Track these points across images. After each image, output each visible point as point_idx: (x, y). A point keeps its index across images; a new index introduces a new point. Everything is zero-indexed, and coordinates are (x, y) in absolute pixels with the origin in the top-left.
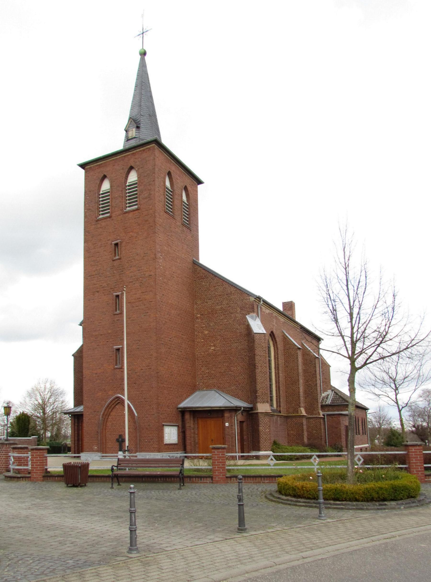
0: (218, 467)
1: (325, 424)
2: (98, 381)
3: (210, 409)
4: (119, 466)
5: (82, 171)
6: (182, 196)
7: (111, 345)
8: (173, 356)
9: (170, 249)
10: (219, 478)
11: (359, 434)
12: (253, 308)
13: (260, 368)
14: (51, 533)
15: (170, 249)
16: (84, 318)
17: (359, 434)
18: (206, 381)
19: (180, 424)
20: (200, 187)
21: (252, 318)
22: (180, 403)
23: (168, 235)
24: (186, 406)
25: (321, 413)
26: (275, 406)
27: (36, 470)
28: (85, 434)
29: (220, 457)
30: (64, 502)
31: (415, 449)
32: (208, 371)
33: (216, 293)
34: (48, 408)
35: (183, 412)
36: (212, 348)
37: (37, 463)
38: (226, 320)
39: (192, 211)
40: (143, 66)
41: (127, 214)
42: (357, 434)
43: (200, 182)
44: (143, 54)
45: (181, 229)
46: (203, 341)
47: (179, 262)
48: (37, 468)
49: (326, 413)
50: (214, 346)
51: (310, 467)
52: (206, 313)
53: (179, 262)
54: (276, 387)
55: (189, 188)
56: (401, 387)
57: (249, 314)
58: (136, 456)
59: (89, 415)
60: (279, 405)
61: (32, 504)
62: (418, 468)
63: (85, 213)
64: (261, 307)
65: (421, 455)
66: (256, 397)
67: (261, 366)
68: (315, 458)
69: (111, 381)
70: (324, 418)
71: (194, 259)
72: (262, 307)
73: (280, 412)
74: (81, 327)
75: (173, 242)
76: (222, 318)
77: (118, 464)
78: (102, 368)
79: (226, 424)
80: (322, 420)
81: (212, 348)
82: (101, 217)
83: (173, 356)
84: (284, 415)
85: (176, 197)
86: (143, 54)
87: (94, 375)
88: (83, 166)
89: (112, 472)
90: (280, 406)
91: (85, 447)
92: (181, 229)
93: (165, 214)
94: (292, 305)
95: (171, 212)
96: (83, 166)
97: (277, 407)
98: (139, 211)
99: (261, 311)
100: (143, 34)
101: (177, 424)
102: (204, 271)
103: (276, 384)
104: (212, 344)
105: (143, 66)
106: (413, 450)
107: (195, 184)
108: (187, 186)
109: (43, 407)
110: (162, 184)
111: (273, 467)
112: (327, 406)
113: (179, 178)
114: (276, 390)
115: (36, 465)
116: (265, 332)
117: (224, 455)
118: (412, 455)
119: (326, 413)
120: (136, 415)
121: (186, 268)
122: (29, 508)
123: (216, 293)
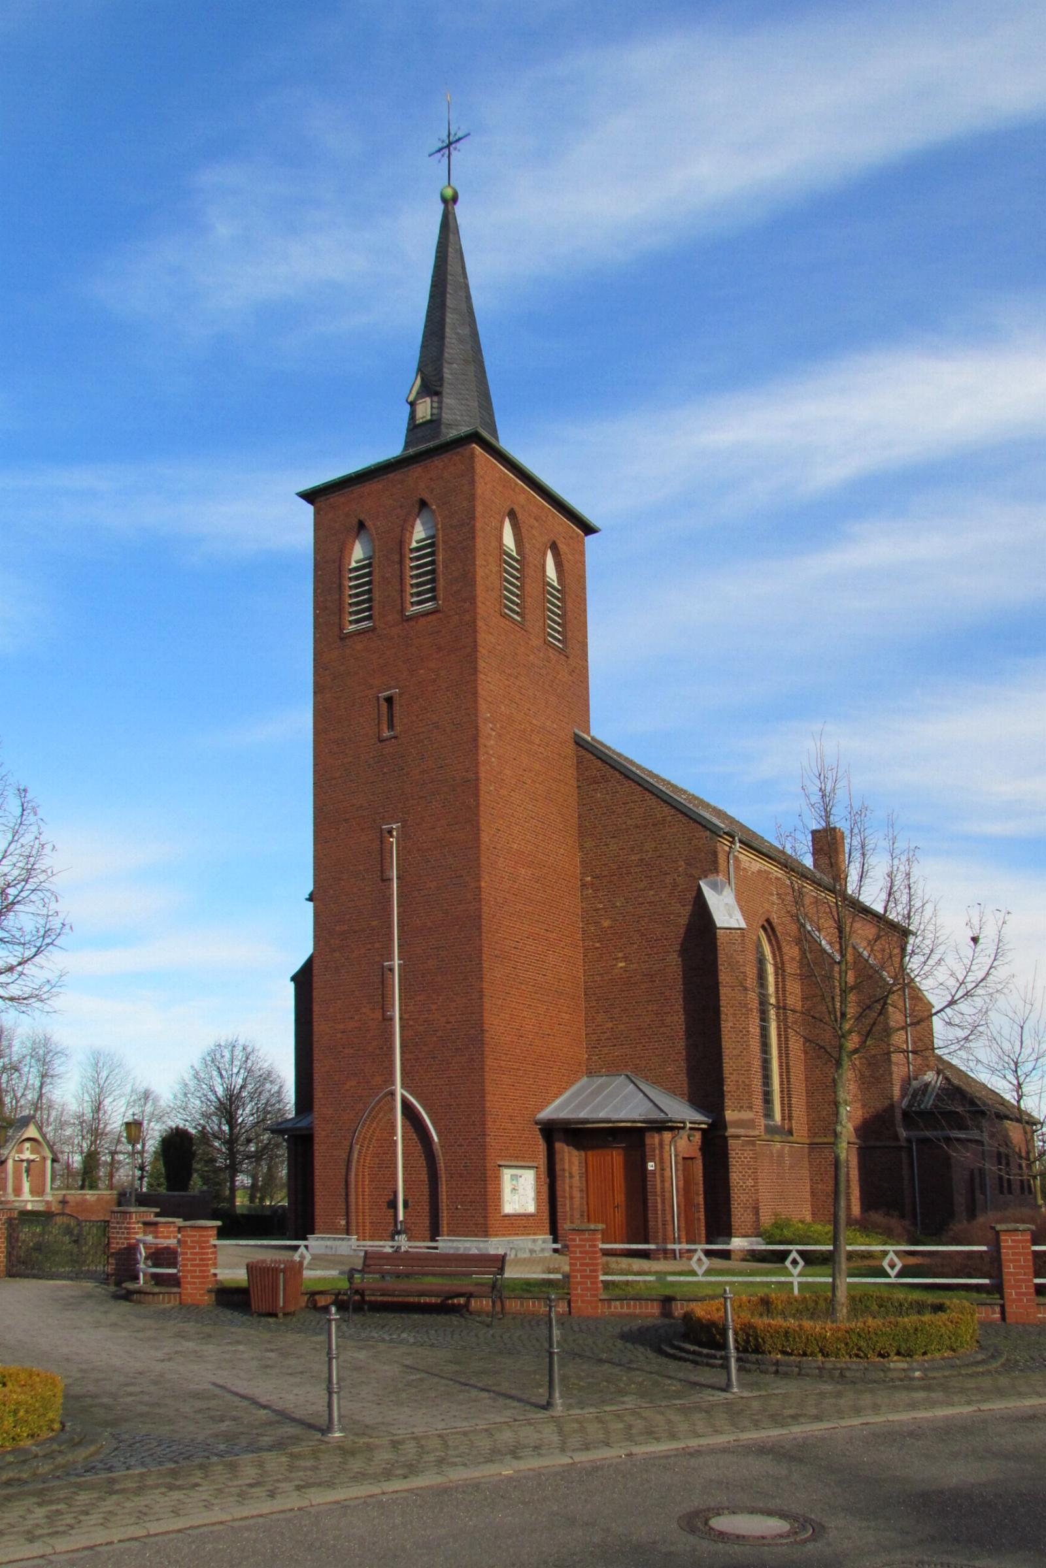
0: (582, 1277)
1: (911, 1165)
2: (346, 1051)
3: (629, 1125)
4: (367, 1269)
5: (310, 509)
6: (544, 571)
7: (377, 959)
8: (523, 987)
9: (513, 711)
10: (583, 1301)
11: (1010, 1192)
12: (715, 862)
13: (731, 1018)
14: (198, 1404)
15: (513, 711)
16: (315, 887)
17: (1010, 1192)
18: (605, 1050)
19: (542, 1160)
20: (590, 540)
21: (714, 887)
22: (542, 1109)
23: (510, 675)
24: (554, 1116)
25: (903, 1133)
26: (778, 1116)
27: (193, 1277)
28: (318, 1186)
29: (586, 1252)
30: (241, 1348)
31: (1013, 1241)
32: (610, 1025)
33: (629, 822)
34: (240, 1112)
35: (553, 1132)
36: (621, 965)
37: (1016, 1247)
38: (652, 893)
39: (570, 605)
40: (448, 227)
41: (412, 623)
42: (1002, 1192)
43: (588, 529)
44: (449, 202)
45: (541, 655)
46: (598, 945)
47: (537, 741)
48: (195, 1271)
49: (915, 1134)
50: (625, 959)
51: (783, 1279)
52: (606, 873)
53: (537, 741)
54: (781, 1066)
55: (563, 547)
56: (1028, 1080)
57: (706, 877)
58: (436, 1248)
59: (327, 1136)
60: (788, 1115)
61: (176, 1352)
62: (1020, 1287)
63: (316, 617)
64: (736, 859)
65: (1027, 1254)
66: (721, 1095)
67: (734, 1015)
68: (700, 1259)
69: (378, 1052)
70: (910, 1149)
71: (577, 731)
72: (741, 856)
73: (790, 1132)
74: (311, 904)
75: (523, 691)
76: (641, 886)
77: (365, 1264)
78: (357, 1017)
79: (650, 1164)
80: (904, 1155)
81: (621, 965)
82: (352, 628)
83: (523, 987)
84: (800, 1140)
85: (530, 571)
86: (449, 202)
87: (339, 1035)
88: (309, 496)
89: (351, 1283)
90: (790, 1118)
91: (319, 1221)
92: (541, 655)
93: (502, 619)
94: (834, 838)
95: (517, 613)
96: (309, 496)
97: (783, 1119)
98: (440, 615)
99: (737, 867)
100: (448, 146)
101: (535, 1164)
102: (599, 763)
103: (780, 1057)
104: (620, 955)
105: (448, 227)
106: (1010, 1243)
107: (578, 535)
108: (558, 542)
109: (228, 1107)
110: (494, 544)
111: (701, 1278)
112: (921, 1114)
113: (536, 524)
114: (781, 1075)
115: (192, 1265)
116: (743, 925)
117: (595, 1246)
118: (1008, 1254)
119: (915, 1134)
120: (436, 1139)
121: (556, 757)
122: (170, 1360)
123: (629, 822)
